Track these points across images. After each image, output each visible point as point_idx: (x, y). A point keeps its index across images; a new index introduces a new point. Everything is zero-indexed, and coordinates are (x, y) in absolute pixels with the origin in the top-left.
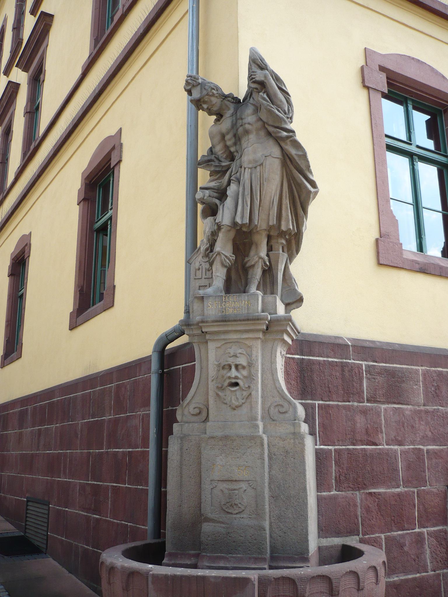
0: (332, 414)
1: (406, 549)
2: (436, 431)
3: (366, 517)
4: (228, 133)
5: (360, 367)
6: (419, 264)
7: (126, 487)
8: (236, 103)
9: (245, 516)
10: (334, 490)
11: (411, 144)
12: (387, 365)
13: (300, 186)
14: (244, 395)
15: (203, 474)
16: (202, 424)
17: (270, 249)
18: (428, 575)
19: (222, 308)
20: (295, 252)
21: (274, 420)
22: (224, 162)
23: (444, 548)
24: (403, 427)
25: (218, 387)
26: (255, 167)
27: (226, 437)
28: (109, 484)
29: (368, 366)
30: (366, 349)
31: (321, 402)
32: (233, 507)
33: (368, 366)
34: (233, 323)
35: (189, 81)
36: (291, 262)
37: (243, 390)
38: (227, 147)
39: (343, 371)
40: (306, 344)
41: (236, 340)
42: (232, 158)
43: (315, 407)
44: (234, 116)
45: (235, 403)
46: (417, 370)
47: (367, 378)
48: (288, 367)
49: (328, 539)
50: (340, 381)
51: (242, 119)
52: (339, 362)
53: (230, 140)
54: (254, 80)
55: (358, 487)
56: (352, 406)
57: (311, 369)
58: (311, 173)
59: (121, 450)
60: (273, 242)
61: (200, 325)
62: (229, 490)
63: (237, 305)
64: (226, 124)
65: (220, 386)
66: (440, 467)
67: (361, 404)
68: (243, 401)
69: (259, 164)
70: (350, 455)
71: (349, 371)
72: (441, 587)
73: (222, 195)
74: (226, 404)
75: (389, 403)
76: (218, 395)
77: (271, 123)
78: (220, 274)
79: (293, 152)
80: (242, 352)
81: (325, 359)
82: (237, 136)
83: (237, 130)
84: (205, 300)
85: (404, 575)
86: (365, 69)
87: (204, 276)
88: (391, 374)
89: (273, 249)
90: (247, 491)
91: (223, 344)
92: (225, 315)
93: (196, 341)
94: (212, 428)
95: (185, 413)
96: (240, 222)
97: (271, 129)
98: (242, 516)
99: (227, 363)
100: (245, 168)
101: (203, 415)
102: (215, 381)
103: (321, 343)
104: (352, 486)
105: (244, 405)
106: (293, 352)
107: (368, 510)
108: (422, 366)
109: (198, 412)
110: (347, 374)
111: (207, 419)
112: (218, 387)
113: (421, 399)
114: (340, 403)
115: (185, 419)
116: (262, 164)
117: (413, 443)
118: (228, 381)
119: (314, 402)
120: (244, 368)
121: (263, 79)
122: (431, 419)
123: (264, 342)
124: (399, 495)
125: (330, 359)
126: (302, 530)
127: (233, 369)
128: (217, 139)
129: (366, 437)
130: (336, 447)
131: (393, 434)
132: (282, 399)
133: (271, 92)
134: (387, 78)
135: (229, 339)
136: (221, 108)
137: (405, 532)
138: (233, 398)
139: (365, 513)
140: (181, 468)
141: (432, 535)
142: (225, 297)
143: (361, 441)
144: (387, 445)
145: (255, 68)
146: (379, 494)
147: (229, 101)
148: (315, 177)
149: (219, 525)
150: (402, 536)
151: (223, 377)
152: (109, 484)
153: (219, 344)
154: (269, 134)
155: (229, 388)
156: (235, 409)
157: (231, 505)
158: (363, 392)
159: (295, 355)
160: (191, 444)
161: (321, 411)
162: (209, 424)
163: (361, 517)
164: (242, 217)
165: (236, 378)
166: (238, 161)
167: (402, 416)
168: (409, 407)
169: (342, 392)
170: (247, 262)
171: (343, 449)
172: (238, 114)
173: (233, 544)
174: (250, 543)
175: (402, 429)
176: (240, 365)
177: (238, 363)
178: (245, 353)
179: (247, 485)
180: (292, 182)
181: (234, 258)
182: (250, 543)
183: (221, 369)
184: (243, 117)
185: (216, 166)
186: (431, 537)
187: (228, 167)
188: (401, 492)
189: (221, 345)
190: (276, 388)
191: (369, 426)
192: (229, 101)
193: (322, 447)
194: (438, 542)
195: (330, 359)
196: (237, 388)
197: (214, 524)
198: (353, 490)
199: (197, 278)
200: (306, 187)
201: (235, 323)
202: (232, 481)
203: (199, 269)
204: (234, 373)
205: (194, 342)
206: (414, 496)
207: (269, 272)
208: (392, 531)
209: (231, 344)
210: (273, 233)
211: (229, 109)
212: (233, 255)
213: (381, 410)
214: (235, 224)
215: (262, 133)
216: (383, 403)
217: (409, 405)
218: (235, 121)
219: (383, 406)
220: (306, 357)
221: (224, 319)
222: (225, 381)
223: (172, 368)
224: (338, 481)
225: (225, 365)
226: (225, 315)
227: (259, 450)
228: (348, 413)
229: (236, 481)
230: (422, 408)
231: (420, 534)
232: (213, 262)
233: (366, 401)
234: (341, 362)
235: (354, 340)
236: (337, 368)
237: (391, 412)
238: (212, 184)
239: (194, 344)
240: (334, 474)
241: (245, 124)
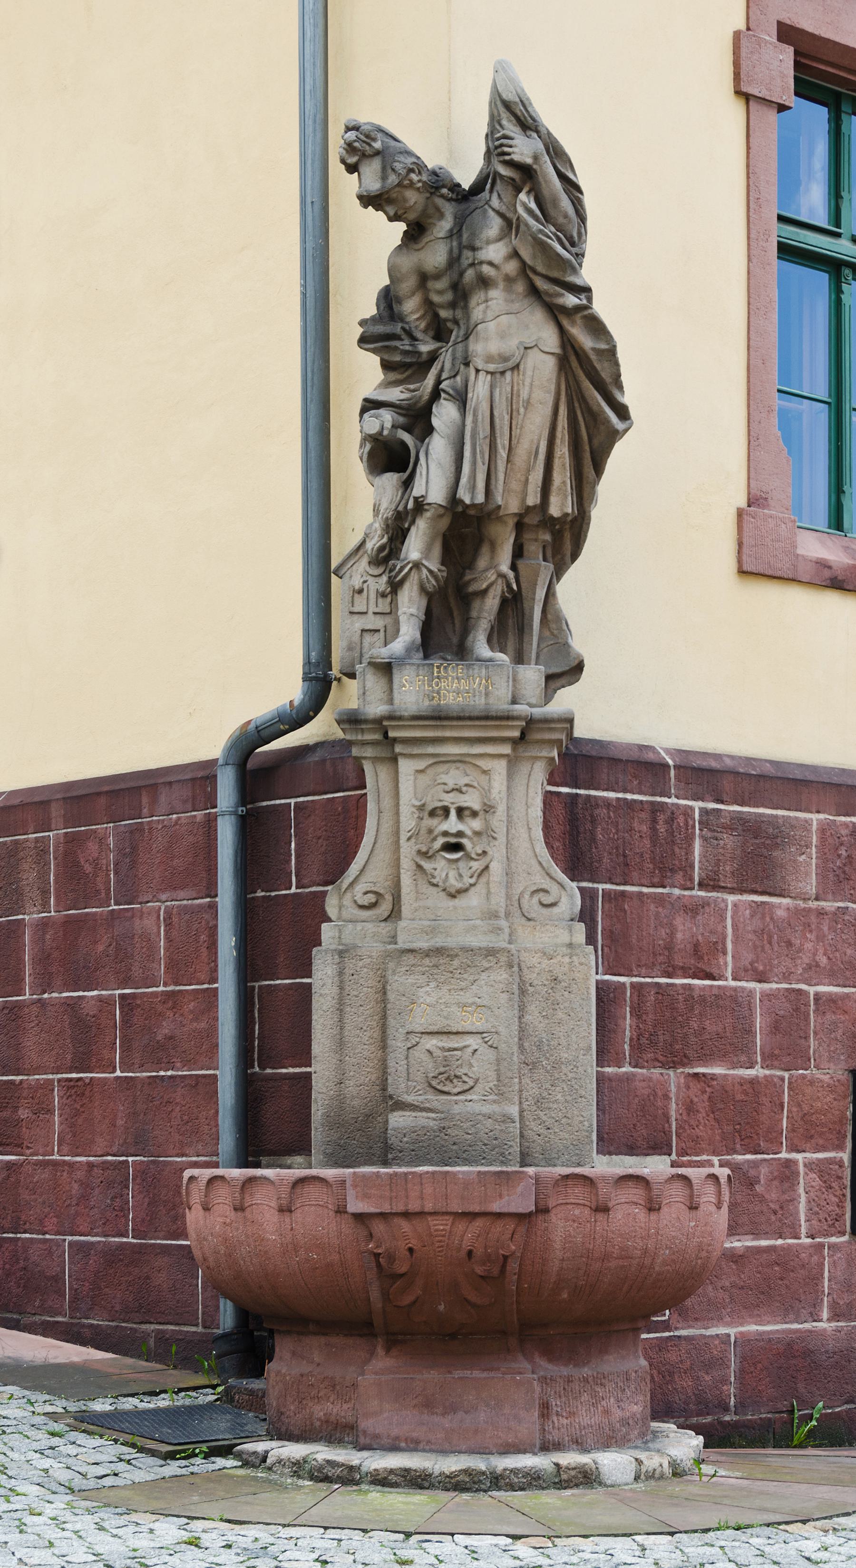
0: (628, 912)
1: (758, 1188)
2: (838, 955)
3: (685, 1121)
4: (437, 277)
5: (688, 812)
6: (830, 567)
7: (118, 1078)
8: (456, 200)
9: (474, 1097)
10: (627, 1065)
11: (838, 235)
12: (746, 809)
13: (594, 418)
14: (474, 869)
15: (391, 1022)
16: (383, 924)
17: (518, 552)
18: (798, 1245)
19: (433, 692)
20: (568, 558)
21: (529, 920)
22: (425, 343)
23: (835, 1196)
24: (770, 943)
25: (419, 852)
26: (503, 373)
27: (439, 951)
28: (50, 1076)
29: (704, 812)
30: (705, 775)
31: (608, 886)
32: (451, 1081)
33: (704, 812)
34: (455, 723)
35: (356, 144)
36: (558, 580)
37: (472, 859)
38: (429, 305)
39: (654, 821)
40: (581, 761)
41: (458, 758)
42: (440, 332)
43: (598, 897)
44: (455, 237)
45: (454, 883)
46: (808, 822)
47: (704, 838)
48: (547, 813)
49: (614, 1157)
50: (647, 842)
51: (474, 249)
52: (647, 802)
53: (440, 292)
54: (507, 158)
55: (674, 1062)
56: (669, 895)
57: (592, 816)
58: (620, 387)
59: (95, 993)
60: (527, 536)
61: (385, 723)
62: (443, 1049)
63: (464, 685)
64: (435, 255)
65: (424, 849)
66: (840, 1031)
67: (687, 893)
68: (472, 881)
69: (510, 364)
70: (660, 997)
71: (666, 822)
72: (823, 1269)
73: (418, 419)
74: (436, 885)
75: (742, 891)
76: (419, 867)
77: (540, 268)
78: (410, 605)
79: (586, 342)
80: (471, 783)
81: (620, 795)
82: (460, 287)
83: (461, 274)
84: (395, 671)
85: (753, 1240)
86: (744, 42)
87: (373, 608)
88: (751, 828)
89: (525, 553)
90: (478, 1053)
91: (431, 765)
92: (439, 705)
93: (369, 755)
94: (409, 932)
95: (345, 903)
96: (467, 501)
97: (540, 284)
98: (469, 1097)
99: (440, 804)
100: (478, 371)
101: (389, 906)
102: (413, 840)
103: (615, 761)
104: (661, 1058)
105: (473, 889)
106: (557, 780)
107: (690, 1108)
108: (818, 812)
109: (374, 900)
110: (662, 828)
111: (394, 914)
112: (419, 852)
113: (811, 885)
114: (645, 890)
115: (345, 914)
116: (517, 366)
117: (786, 977)
118: (441, 841)
119: (595, 885)
120: (474, 814)
121: (529, 161)
122: (829, 929)
123: (512, 761)
124: (753, 1082)
125: (629, 796)
126: (581, 1122)
127: (453, 813)
128: (408, 284)
129: (693, 962)
130: (635, 979)
131: (748, 957)
132: (547, 878)
133: (546, 192)
134: (797, 65)
135: (444, 755)
136: (424, 213)
137: (759, 1156)
138: (452, 874)
139: (685, 1114)
140: (341, 1011)
141: (814, 1166)
142: (438, 667)
143: (682, 968)
144: (734, 979)
145: (510, 128)
146: (713, 1077)
147: (442, 196)
148: (628, 398)
149: (424, 1114)
150: (755, 1164)
151: (430, 831)
152: (50, 1076)
153: (421, 764)
154: (534, 292)
155: (443, 854)
156: (453, 896)
157: (448, 1079)
158: (692, 866)
159: (562, 786)
160: (361, 964)
161: (607, 906)
162: (402, 924)
163: (676, 1120)
164: (473, 488)
165: (460, 834)
166: (460, 347)
167: (768, 919)
168: (785, 901)
169: (651, 866)
170: (469, 583)
171: (648, 984)
172: (465, 236)
173: (454, 1147)
174: (485, 1145)
175: (767, 946)
176: (467, 808)
177: (465, 805)
178: (475, 784)
179: (480, 1041)
180: (576, 405)
181: (445, 574)
182: (485, 1145)
183: (426, 814)
184: (478, 244)
185: (406, 353)
186: (811, 1170)
187: (433, 357)
188: (757, 1077)
189: (427, 768)
190: (536, 856)
191: (700, 938)
192: (442, 196)
193: (607, 977)
194: (825, 1182)
195: (629, 796)
196: (459, 855)
197: (414, 1114)
198: (663, 1066)
199: (356, 610)
200: (607, 421)
201: (461, 723)
202: (449, 1033)
203: (360, 591)
204: (452, 824)
205: (365, 758)
206: (782, 1086)
207: (513, 604)
208: (735, 1152)
209: (447, 766)
210: (532, 520)
211: (442, 216)
212: (443, 568)
213: (727, 906)
214: (454, 500)
215: (520, 287)
216: (732, 891)
217: (784, 897)
218: (456, 251)
219: (731, 898)
220: (582, 792)
221: (436, 714)
222: (435, 839)
223: (265, 804)
224: (637, 1047)
225: (436, 808)
226: (439, 705)
227: (505, 976)
228: (660, 909)
229: (457, 1033)
230: (813, 904)
231: (788, 1163)
232: (402, 582)
233: (696, 887)
234: (652, 803)
235: (680, 752)
236: (643, 815)
237: (748, 912)
238: (396, 394)
239: (364, 762)
240: (628, 1033)
241: (481, 263)
